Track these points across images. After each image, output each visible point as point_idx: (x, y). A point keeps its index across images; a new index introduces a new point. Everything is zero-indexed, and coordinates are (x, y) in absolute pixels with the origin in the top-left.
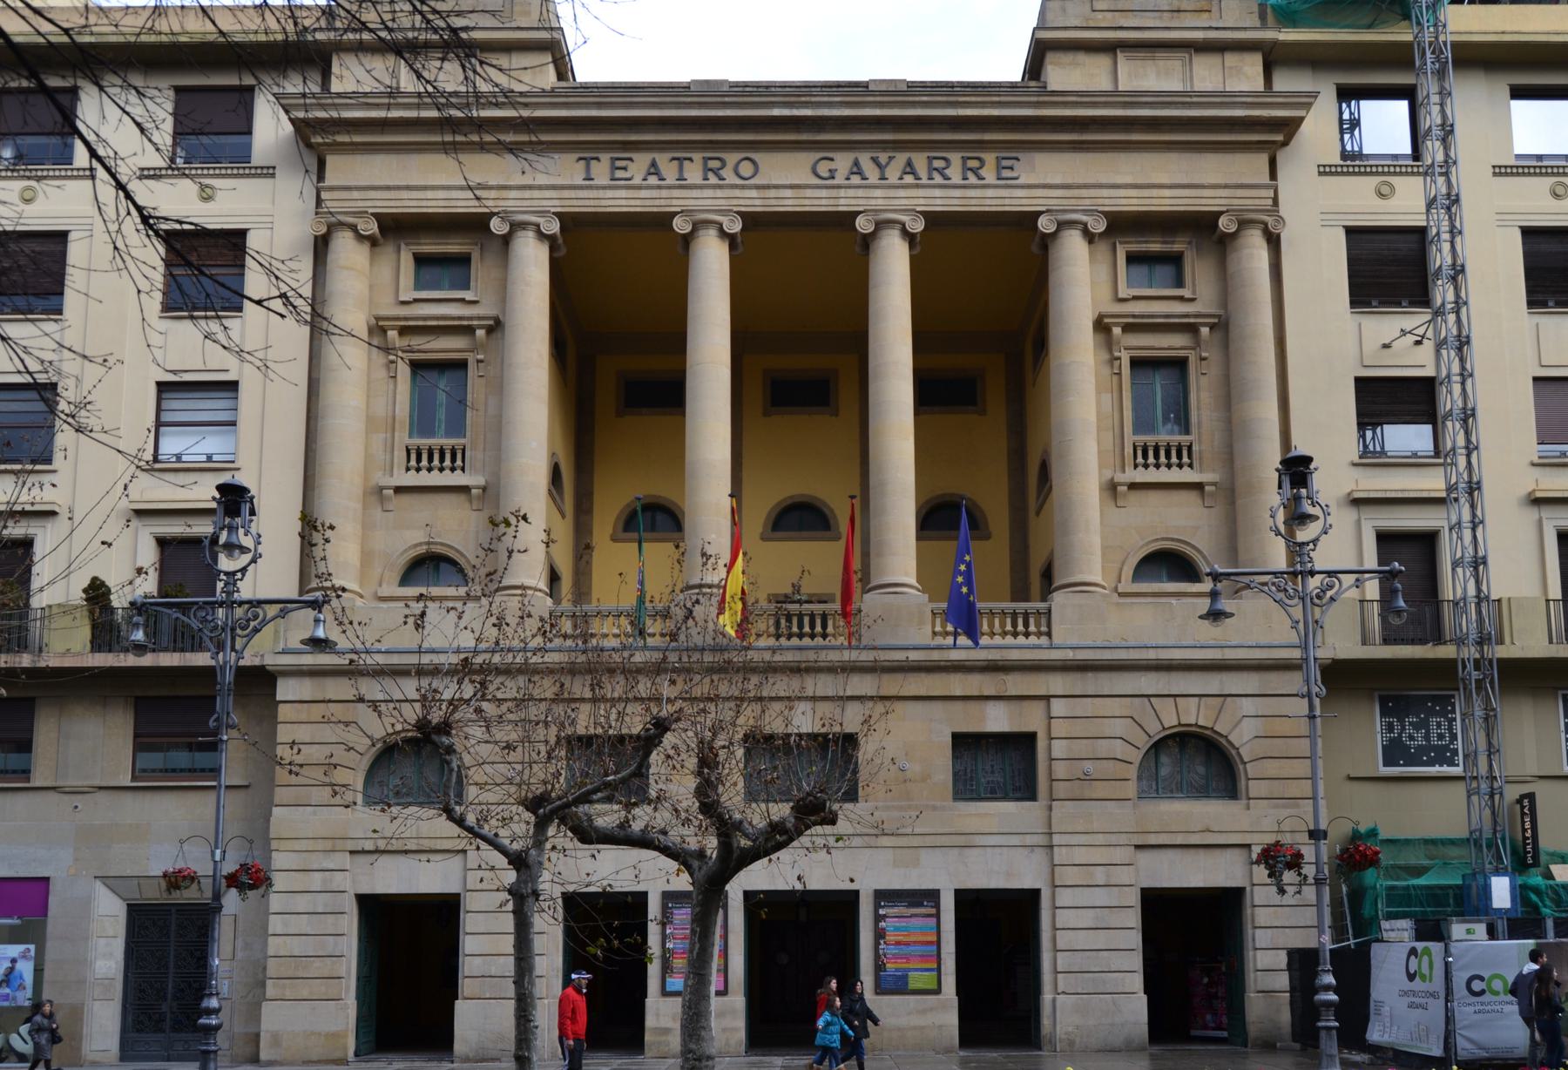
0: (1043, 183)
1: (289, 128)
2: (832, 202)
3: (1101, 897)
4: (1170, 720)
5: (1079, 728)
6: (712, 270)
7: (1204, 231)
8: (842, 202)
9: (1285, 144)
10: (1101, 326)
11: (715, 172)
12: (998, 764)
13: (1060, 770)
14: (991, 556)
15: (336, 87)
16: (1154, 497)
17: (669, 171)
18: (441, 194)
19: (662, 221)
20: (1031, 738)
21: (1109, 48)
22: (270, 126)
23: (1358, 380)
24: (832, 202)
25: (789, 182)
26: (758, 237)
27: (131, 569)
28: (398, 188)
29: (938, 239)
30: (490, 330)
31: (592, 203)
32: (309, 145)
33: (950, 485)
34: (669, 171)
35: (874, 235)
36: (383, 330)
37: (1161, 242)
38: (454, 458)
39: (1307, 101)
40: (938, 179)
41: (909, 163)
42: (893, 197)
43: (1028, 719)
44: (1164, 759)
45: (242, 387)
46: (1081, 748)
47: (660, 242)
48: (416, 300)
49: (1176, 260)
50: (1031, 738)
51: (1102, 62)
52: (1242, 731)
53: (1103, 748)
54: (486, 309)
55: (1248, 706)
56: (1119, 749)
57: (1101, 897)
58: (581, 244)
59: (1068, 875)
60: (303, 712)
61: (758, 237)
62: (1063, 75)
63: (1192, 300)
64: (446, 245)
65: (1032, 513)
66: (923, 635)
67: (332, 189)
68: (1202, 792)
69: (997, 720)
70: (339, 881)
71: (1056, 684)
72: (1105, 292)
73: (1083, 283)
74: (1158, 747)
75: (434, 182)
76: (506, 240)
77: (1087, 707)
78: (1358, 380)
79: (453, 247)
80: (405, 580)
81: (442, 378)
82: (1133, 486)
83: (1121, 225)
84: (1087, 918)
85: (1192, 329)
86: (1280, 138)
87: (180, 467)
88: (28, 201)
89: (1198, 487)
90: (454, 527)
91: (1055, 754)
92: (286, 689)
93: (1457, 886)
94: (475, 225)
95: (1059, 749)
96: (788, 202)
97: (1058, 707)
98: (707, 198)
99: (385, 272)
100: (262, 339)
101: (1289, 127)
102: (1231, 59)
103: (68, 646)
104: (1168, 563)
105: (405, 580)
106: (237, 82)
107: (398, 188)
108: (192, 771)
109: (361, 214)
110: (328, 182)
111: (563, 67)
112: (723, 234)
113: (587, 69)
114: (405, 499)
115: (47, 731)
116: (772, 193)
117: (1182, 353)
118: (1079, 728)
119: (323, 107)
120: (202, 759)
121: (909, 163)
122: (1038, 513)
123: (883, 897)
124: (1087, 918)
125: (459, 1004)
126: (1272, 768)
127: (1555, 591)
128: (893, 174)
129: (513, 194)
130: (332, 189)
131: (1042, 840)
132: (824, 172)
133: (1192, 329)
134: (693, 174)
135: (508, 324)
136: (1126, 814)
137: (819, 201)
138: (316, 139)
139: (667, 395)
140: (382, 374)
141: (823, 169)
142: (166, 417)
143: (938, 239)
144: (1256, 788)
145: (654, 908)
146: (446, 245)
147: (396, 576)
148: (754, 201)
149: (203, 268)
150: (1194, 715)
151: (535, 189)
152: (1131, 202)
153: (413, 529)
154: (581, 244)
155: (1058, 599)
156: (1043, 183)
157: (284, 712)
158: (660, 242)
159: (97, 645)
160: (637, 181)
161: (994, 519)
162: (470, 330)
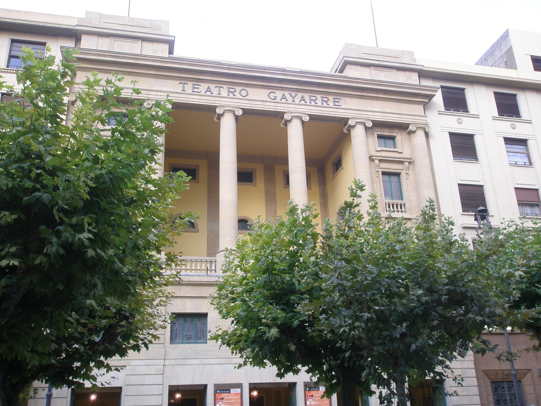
2: (275, 108)
8: (279, 108)
9: (428, 103)
24: (275, 108)
25: (259, 99)
31: (184, 99)
36: (373, 160)
37: (386, 131)
40: (313, 103)
48: (381, 150)
49: (393, 138)
61: (247, 119)
63: (401, 153)
100: (452, 174)
116: (253, 102)
117: (399, 171)
128: (297, 100)
141: (272, 96)
143: (313, 125)
156: (350, 108)
160: (202, 93)
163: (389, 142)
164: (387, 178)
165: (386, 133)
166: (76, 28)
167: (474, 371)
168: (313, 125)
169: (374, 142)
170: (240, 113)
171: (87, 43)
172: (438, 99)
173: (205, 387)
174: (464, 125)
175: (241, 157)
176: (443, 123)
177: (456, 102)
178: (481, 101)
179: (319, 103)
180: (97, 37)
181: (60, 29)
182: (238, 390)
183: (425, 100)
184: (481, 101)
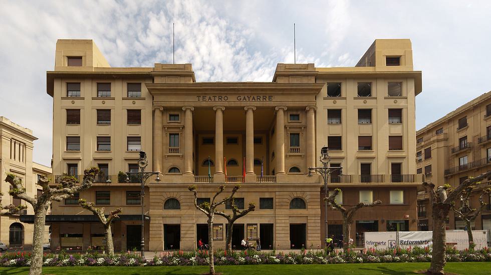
0: (277, 101)
1: (148, 91)
3: (283, 225)
4: (295, 196)
5: (280, 197)
6: (219, 117)
7: (304, 110)
9: (318, 94)
10: (285, 127)
11: (221, 99)
12: (267, 203)
13: (277, 204)
14: (263, 169)
15: (317, 82)
16: (293, 158)
17: (213, 98)
18: (174, 103)
19: (211, 108)
20: (272, 199)
21: (288, 76)
22: (144, 90)
23: (359, 137)
25: (233, 101)
26: (227, 111)
27: (125, 170)
28: (166, 102)
29: (258, 112)
30: (182, 128)
32: (151, 94)
33: (232, 157)
34: (213, 98)
35: (247, 111)
36: (165, 128)
37: (296, 113)
38: (177, 150)
39: (322, 85)
40: (259, 100)
41: (254, 97)
42: (251, 104)
43: (273, 196)
44: (294, 202)
45: (142, 139)
46: (280, 200)
47: (211, 112)
49: (298, 116)
50: (272, 199)
51: (287, 78)
52: (307, 197)
53: (284, 200)
54: (303, 123)
55: (308, 193)
56: (287, 200)
57: (283, 225)
58: (197, 113)
59: (278, 221)
60: (154, 194)
61: (227, 111)
62: (279, 81)
64: (174, 113)
65: (270, 161)
66: (255, 181)
67: (155, 102)
68: (300, 208)
69: (267, 196)
70: (161, 222)
71: (277, 189)
72: (286, 121)
73: (282, 120)
74: (293, 201)
75: (173, 101)
76: (185, 111)
77: (281, 193)
78: (359, 137)
79: (176, 113)
80: (169, 172)
81: (174, 135)
82: (290, 156)
83: (290, 109)
84: (281, 228)
85: (301, 128)
86: (317, 92)
87: (132, 152)
88: (134, 104)
89: (301, 156)
90: (176, 162)
91: (276, 201)
92: (151, 190)
93: (22, 239)
94: (179, 109)
95: (277, 200)
96: (233, 104)
97: (277, 193)
98: (219, 104)
99: (286, 118)
100: (144, 130)
101: (319, 90)
102: (309, 78)
103: (115, 182)
104: (295, 169)
105: (169, 172)
106: (287, 82)
107: (166, 102)
108: (136, 204)
109: (161, 106)
110: (154, 100)
111: (194, 81)
112: (191, 111)
113: (198, 80)
114: (169, 158)
115: (112, 197)
117: (298, 132)
118: (280, 197)
119: (153, 86)
120: (107, 201)
121: (254, 97)
122: (272, 161)
123: (248, 225)
124: (281, 228)
125: (181, 242)
126: (312, 204)
127: (360, 174)
128: (251, 99)
129: (186, 103)
130: (155, 102)
131: (274, 215)
132: (239, 98)
133: (301, 128)
134: (217, 99)
135: (186, 126)
136: (287, 211)
137: (238, 104)
138: (153, 93)
139: (211, 141)
140: (164, 135)
141: (239, 98)
142: (99, 143)
143: (258, 112)
144: (309, 207)
145: (245, 225)
146: (174, 113)
147: (168, 171)
148: (227, 104)
149: (134, 117)
150: (299, 195)
151: (191, 102)
152: (291, 104)
153: (170, 163)
154: (197, 113)
155: (278, 175)
156: (277, 101)
157: (151, 194)
158: (211, 112)
159: (120, 181)
161: (266, 161)
162: (179, 128)
163: (176, 118)
164: (292, 136)
165: (294, 113)
166: (152, 73)
167: (150, 226)
168: (259, 113)
169: (166, 118)
170: (224, 109)
171: (157, 81)
172: (324, 91)
173: (244, 224)
174: (338, 104)
175: (256, 132)
176: (324, 103)
177: (335, 92)
178: (350, 90)
179: (262, 100)
180: (179, 77)
181: (126, 75)
182: (222, 226)
183: (316, 92)
184: (350, 90)
